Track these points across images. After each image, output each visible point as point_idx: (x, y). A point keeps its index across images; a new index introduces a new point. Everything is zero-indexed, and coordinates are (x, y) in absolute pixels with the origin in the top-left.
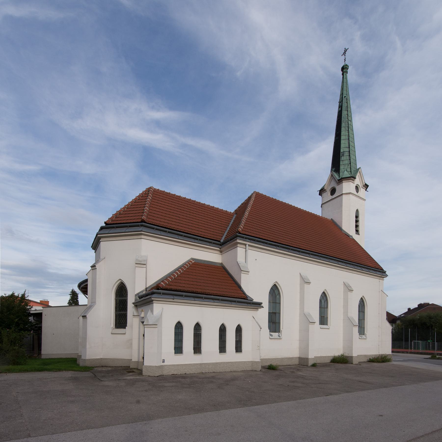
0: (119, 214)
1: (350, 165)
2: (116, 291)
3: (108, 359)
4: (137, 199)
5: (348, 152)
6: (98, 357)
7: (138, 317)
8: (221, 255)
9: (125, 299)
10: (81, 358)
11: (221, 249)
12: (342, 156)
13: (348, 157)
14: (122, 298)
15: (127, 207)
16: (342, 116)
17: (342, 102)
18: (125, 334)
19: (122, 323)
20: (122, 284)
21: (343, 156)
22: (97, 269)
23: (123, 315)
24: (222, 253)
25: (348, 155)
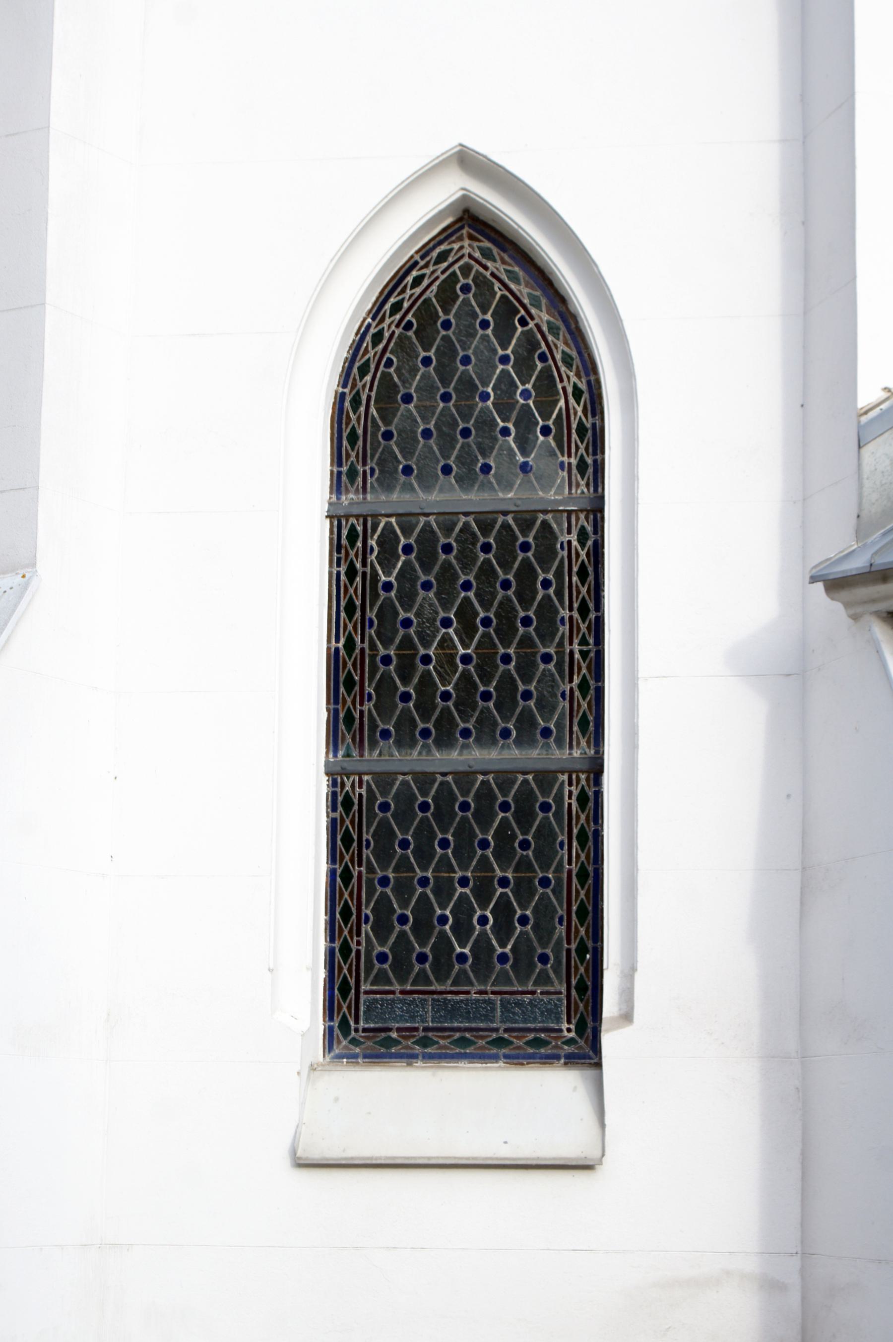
2: (346, 377)
9: (526, 520)
19: (482, 949)
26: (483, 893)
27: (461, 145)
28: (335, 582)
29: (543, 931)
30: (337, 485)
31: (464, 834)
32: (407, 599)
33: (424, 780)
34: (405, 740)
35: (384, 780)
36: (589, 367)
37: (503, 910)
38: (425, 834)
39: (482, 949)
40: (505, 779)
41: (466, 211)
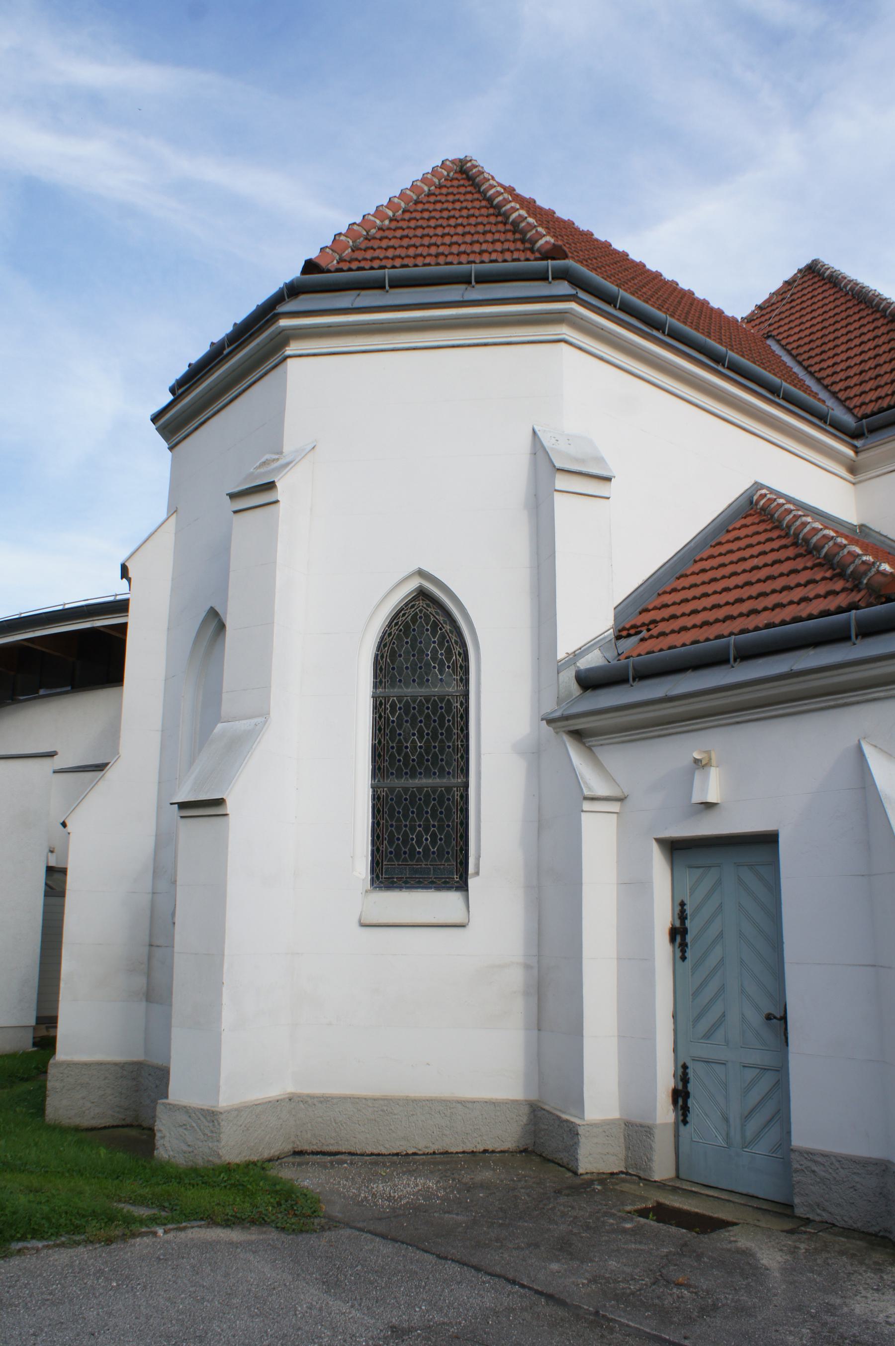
0: (366, 239)
3: (344, 1099)
4: (424, 191)
6: (274, 1091)
7: (615, 807)
8: (854, 484)
9: (442, 698)
10: (167, 1097)
11: (862, 456)
14: (423, 691)
15: (390, 213)
18: (462, 926)
19: (426, 849)
20: (421, 603)
22: (282, 505)
23: (427, 803)
24: (861, 477)
26: (427, 830)
27: (421, 573)
28: (374, 719)
29: (448, 843)
30: (375, 686)
31: (420, 808)
32: (400, 726)
33: (406, 790)
34: (399, 775)
35: (392, 790)
36: (464, 645)
37: (434, 836)
38: (406, 809)
39: (426, 849)
40: (434, 789)
41: (422, 594)
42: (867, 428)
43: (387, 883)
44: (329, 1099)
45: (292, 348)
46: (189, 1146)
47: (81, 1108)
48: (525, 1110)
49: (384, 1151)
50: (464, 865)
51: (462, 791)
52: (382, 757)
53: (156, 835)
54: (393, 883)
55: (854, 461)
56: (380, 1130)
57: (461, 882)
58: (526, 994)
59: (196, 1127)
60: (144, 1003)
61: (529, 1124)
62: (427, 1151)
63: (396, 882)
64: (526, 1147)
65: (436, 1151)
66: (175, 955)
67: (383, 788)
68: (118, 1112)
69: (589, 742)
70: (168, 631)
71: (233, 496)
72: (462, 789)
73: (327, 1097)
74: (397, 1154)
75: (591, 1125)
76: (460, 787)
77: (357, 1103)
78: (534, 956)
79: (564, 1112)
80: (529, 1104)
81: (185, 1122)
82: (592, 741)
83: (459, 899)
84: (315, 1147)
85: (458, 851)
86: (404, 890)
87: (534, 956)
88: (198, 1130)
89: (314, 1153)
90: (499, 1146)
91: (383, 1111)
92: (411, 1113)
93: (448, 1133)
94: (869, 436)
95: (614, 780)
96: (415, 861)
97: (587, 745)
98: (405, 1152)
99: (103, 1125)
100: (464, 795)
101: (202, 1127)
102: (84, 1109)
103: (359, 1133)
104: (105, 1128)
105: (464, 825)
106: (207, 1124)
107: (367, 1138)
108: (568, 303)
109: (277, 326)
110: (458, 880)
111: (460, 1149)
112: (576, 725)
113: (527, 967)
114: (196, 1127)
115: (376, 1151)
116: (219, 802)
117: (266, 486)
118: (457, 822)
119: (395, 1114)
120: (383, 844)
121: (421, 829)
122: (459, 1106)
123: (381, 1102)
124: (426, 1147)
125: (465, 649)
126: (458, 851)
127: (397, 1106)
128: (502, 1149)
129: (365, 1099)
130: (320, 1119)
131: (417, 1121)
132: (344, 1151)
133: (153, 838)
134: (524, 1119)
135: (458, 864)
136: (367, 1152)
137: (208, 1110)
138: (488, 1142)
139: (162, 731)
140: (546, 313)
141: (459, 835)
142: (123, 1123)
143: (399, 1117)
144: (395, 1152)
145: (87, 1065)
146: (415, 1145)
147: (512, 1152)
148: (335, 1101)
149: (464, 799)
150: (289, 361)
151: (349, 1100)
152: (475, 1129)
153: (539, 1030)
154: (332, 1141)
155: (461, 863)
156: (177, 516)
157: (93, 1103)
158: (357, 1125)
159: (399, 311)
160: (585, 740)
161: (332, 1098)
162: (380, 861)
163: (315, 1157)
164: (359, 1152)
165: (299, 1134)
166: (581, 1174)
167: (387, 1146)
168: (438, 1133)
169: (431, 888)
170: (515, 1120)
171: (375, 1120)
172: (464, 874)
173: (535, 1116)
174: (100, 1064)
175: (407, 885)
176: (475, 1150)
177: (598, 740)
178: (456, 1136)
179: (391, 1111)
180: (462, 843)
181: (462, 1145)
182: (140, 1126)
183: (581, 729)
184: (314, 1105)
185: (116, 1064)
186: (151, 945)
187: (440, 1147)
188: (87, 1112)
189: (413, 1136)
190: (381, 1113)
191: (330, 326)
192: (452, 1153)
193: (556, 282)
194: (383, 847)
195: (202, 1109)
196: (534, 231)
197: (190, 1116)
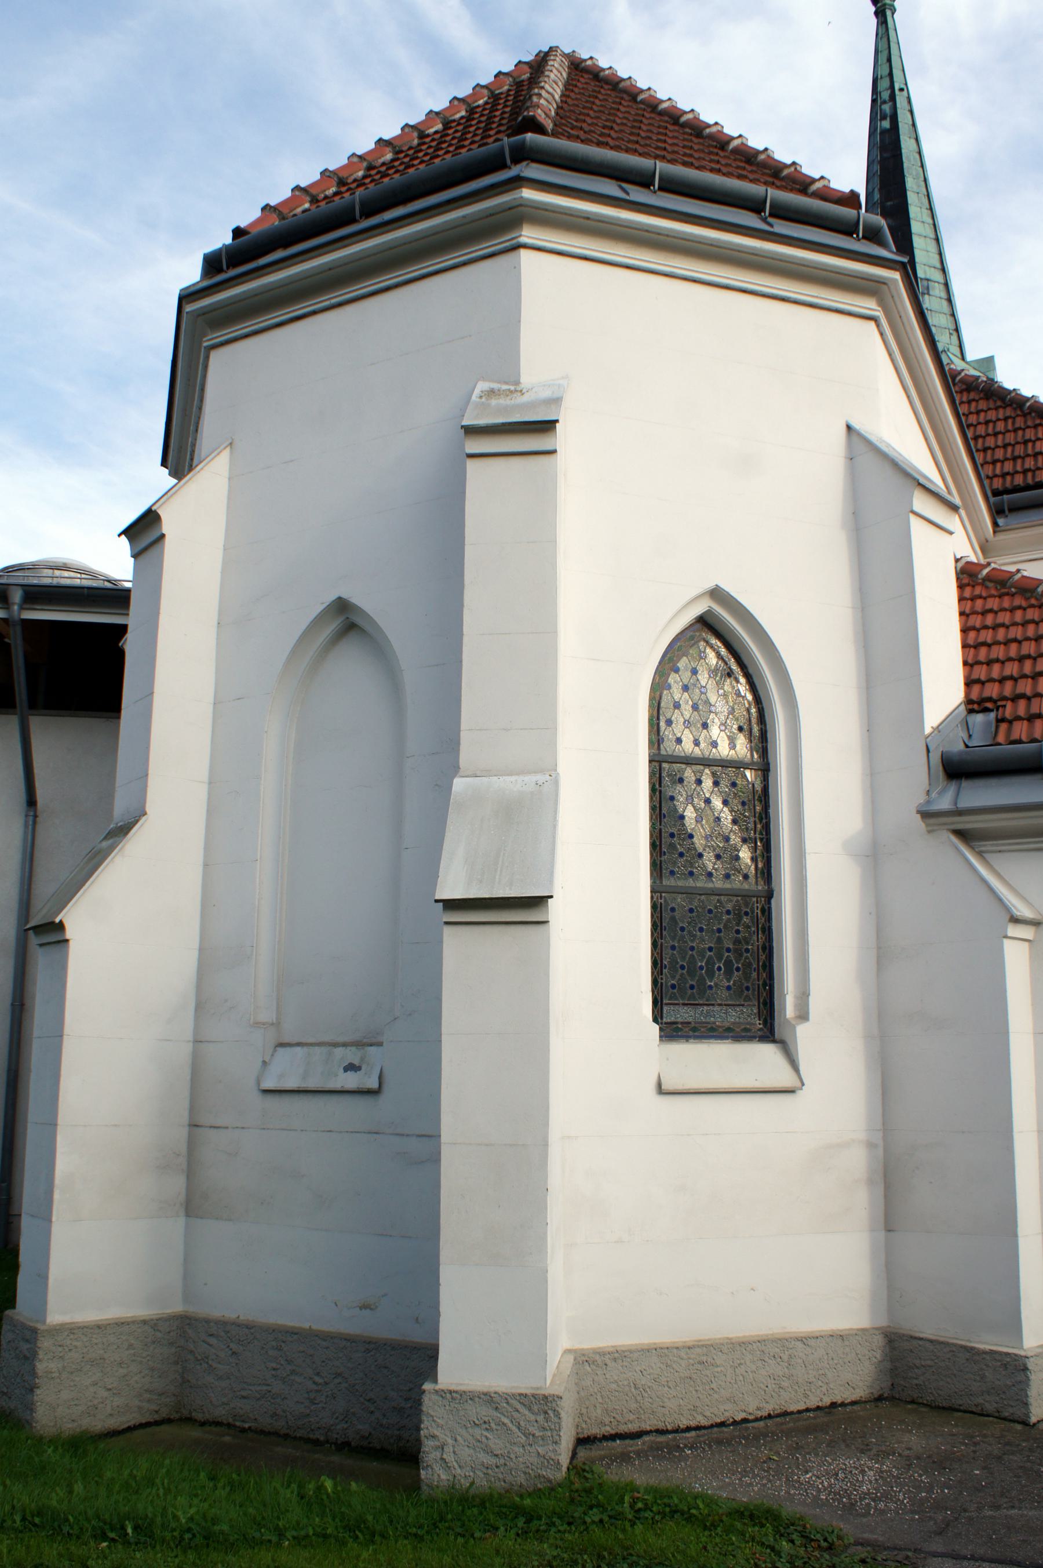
1: (955, 334)
5: (942, 287)
10: (435, 1380)
11: (1001, 537)
12: (923, 294)
13: (945, 303)
16: (903, 151)
17: (891, 103)
18: (790, 1091)
21: (928, 294)
25: (944, 295)
42: (1009, 505)
43: (668, 1030)
44: (626, 1354)
45: (528, 234)
46: (496, 1455)
47: (91, 1401)
48: (879, 1341)
49: (704, 1422)
50: (768, 1005)
51: (763, 902)
52: (658, 848)
53: (201, 950)
54: (677, 1030)
55: (987, 541)
56: (696, 1391)
57: (765, 1030)
58: (870, 1182)
59: (510, 1425)
60: (182, 1221)
61: (884, 1360)
62: (759, 1414)
63: (681, 1030)
64: (881, 1392)
65: (772, 1413)
66: (442, 1145)
67: (661, 893)
68: (149, 1401)
69: (981, 846)
70: (218, 627)
71: (471, 431)
72: (763, 899)
73: (624, 1351)
74: (722, 1424)
75: (239, 1326)
76: (760, 897)
77: (666, 1355)
78: (879, 1130)
79: (970, 1342)
80: (883, 1333)
81: (486, 1419)
82: (984, 846)
83: (775, 1053)
84: (608, 1428)
85: (761, 987)
86: (692, 1041)
87: (879, 1130)
88: (514, 1428)
89: (606, 1438)
90: (849, 1396)
91: (701, 1363)
92: (739, 1362)
93: (786, 1384)
94: (1009, 516)
95: (1028, 901)
96: (705, 999)
97: (977, 850)
98: (731, 1420)
99: (125, 1426)
100: (766, 908)
101: (522, 1423)
102: (96, 1402)
103: (669, 1399)
104: (129, 1429)
105: (767, 951)
106: (533, 1417)
107: (680, 1405)
108: (892, 272)
109: (516, 196)
110: (761, 1026)
111: (801, 1406)
112: (969, 822)
113: (871, 1145)
114: (510, 1425)
115: (693, 1424)
116: (538, 902)
117: (539, 426)
118: (758, 946)
119: (717, 1366)
120: (662, 974)
121: (712, 953)
122: (799, 1344)
123: (698, 1350)
124: (758, 1409)
125: (760, 706)
126: (761, 987)
127: (720, 1353)
128: (853, 1399)
129: (677, 1348)
130: (614, 1386)
131: (747, 1372)
132: (649, 1428)
133: (196, 953)
134: (878, 1355)
135: (761, 1005)
136: (682, 1426)
137: (533, 1396)
138: (836, 1392)
139: (210, 783)
140: (863, 278)
141: (761, 964)
142: (157, 1417)
143: (723, 1369)
144: (719, 1421)
145: (99, 1327)
146: (744, 1407)
147: (865, 1402)
148: (636, 1355)
149: (767, 913)
150: (523, 252)
151: (654, 1351)
152: (819, 1375)
153: (889, 1231)
154: (632, 1417)
155: (765, 1004)
156: (231, 453)
157: (110, 1389)
158: (666, 1388)
159: (686, 222)
160: (974, 844)
161: (631, 1351)
162: (659, 999)
163: (610, 1444)
164: (669, 1428)
165: (584, 1411)
166: (1034, 1424)
167: (708, 1414)
168: (774, 1386)
169: (727, 1038)
170: (867, 1357)
171: (690, 1378)
172: (768, 1019)
173: (893, 1349)
174: (120, 1324)
175: (696, 1034)
176: (820, 1404)
177: (997, 845)
178: (797, 1388)
179: (712, 1361)
180: (764, 975)
181: (804, 1400)
182: (189, 1420)
183: (970, 829)
184: (606, 1365)
185: (145, 1322)
186: (194, 1125)
187: (777, 1407)
188: (101, 1406)
189: (741, 1396)
190: (699, 1367)
191: (587, 217)
192: (792, 1413)
193: (864, 241)
194: (662, 979)
195: (520, 1395)
196: (792, 169)
197: (497, 1408)
